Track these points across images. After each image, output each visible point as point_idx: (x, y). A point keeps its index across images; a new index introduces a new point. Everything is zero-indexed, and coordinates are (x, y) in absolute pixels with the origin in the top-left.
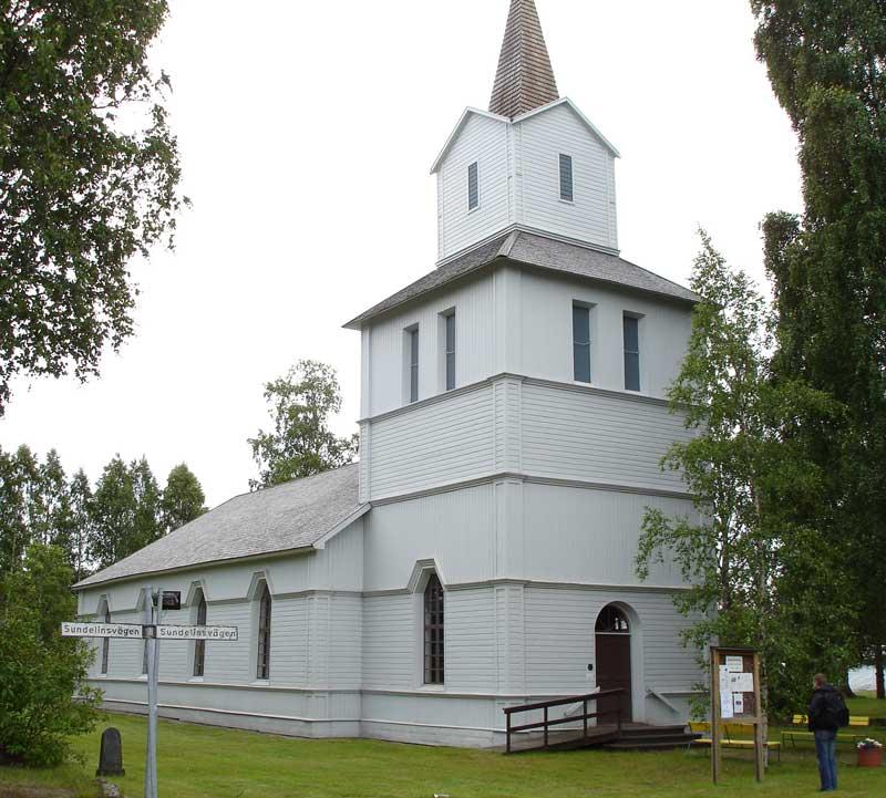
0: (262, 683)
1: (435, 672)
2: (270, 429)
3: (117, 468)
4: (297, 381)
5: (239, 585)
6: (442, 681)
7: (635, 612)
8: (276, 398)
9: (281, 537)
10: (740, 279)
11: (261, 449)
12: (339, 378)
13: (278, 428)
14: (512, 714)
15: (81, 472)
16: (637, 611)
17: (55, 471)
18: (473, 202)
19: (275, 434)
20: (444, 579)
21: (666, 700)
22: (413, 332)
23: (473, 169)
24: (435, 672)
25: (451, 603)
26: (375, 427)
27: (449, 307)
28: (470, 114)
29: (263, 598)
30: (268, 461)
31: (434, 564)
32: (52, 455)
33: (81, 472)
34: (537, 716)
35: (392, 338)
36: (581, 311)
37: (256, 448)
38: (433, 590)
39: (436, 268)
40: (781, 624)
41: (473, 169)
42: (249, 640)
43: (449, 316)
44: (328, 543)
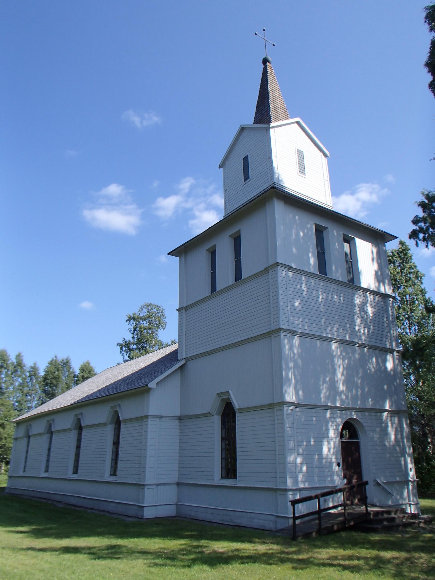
0: (112, 479)
1: (230, 470)
2: (129, 337)
3: (53, 363)
4: (145, 313)
5: (102, 414)
6: (235, 477)
7: (363, 425)
8: (133, 323)
9: (128, 383)
10: (422, 205)
11: (124, 349)
12: (166, 313)
13: (133, 338)
14: (296, 505)
15: (35, 364)
16: (364, 424)
17: (19, 364)
18: (246, 177)
19: (131, 340)
20: (236, 405)
21: (386, 487)
22: (213, 253)
23: (246, 160)
24: (230, 470)
25: (242, 422)
26: (188, 312)
27: (236, 230)
28: (243, 129)
29: (116, 422)
30: (128, 355)
31: (229, 395)
32: (19, 356)
33: (35, 364)
34: (314, 505)
35: (201, 257)
36: (320, 231)
37: (121, 348)
38: (228, 414)
39: (223, 218)
40: (5, 472)
41: (246, 160)
42: (413, 512)
43: (237, 240)
44: (157, 384)
